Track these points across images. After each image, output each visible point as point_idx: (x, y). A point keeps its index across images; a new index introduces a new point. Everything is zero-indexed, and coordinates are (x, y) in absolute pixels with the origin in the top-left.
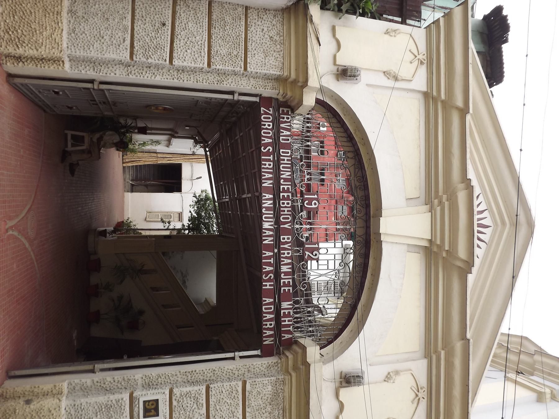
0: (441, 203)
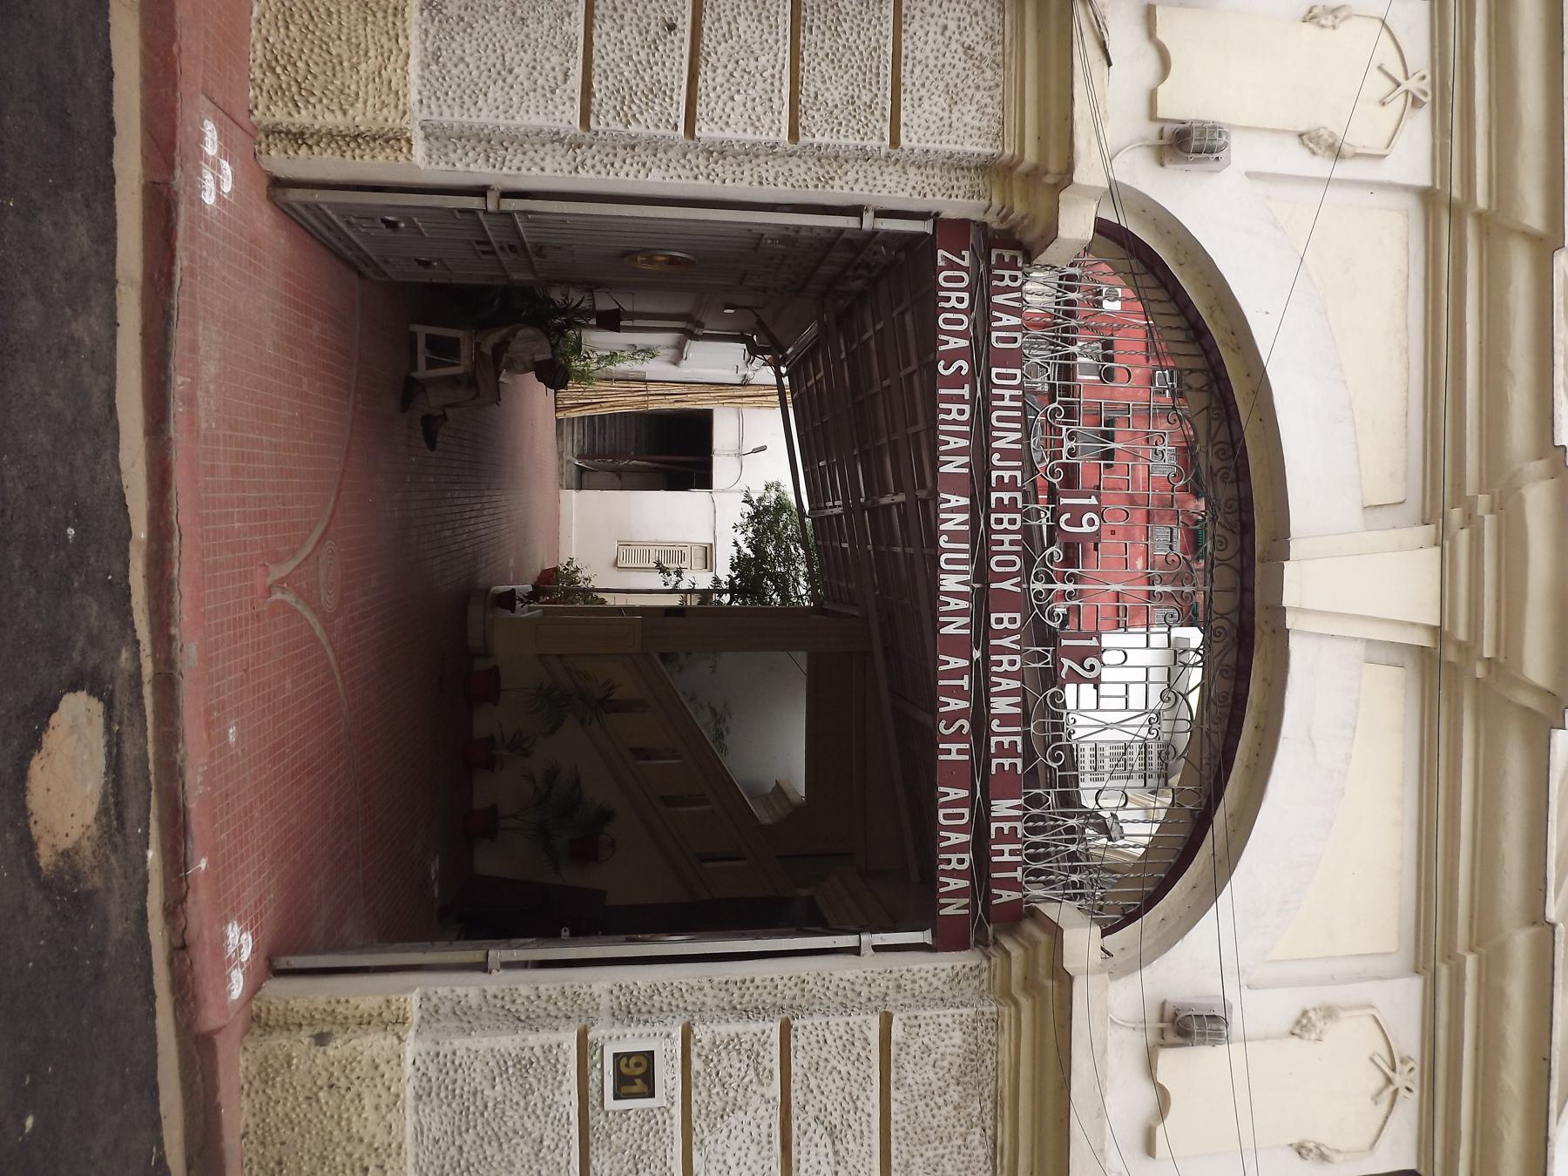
0: (1470, 518)
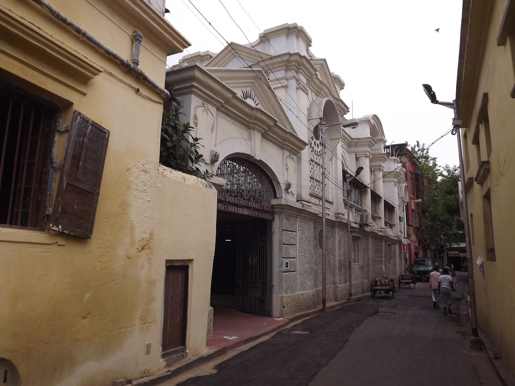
0: (254, 124)
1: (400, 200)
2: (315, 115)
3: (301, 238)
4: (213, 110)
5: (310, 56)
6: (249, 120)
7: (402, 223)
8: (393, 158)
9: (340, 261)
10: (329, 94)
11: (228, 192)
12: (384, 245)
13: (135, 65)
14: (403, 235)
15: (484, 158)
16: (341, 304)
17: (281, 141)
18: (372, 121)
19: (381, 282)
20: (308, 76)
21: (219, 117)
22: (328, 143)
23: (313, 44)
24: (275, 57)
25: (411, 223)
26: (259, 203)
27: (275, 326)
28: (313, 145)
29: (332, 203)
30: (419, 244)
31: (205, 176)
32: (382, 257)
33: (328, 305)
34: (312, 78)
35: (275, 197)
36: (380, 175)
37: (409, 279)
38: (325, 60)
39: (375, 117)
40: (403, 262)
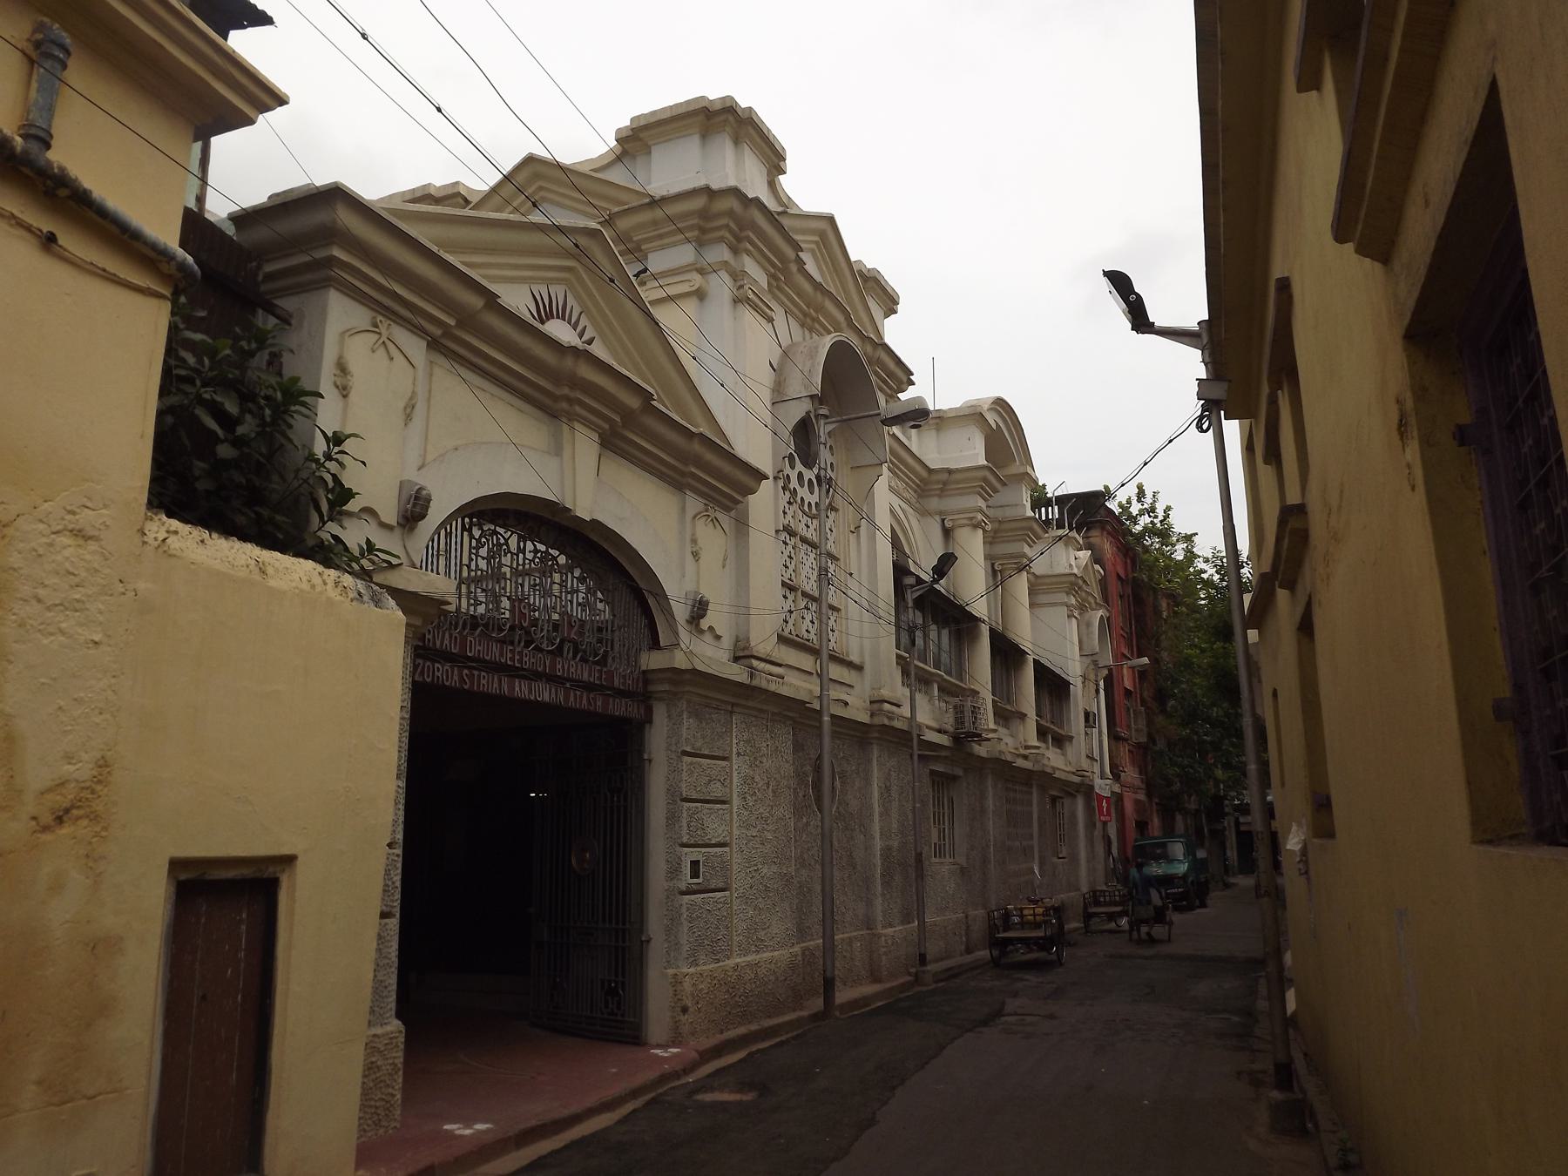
0: (570, 400)
1: (1088, 660)
2: (796, 388)
3: (748, 780)
4: (415, 347)
5: (781, 203)
6: (552, 388)
7: (1095, 731)
8: (1060, 532)
9: (886, 852)
10: (844, 324)
11: (474, 627)
12: (1035, 802)
13: (34, 147)
14: (1097, 769)
15: (1293, 498)
16: (891, 989)
17: (672, 461)
18: (992, 418)
19: (1022, 916)
20: (773, 265)
21: (438, 371)
22: (843, 479)
23: (790, 163)
24: (664, 199)
25: (1123, 733)
26: (596, 663)
27: (651, 1075)
28: (794, 483)
29: (859, 668)
30: (1149, 795)
31: (363, 566)
32: (1031, 837)
33: (842, 996)
34: (785, 271)
35: (655, 644)
36: (1021, 584)
37: (1116, 904)
38: (831, 220)
39: (1001, 405)
40: (1100, 849)
